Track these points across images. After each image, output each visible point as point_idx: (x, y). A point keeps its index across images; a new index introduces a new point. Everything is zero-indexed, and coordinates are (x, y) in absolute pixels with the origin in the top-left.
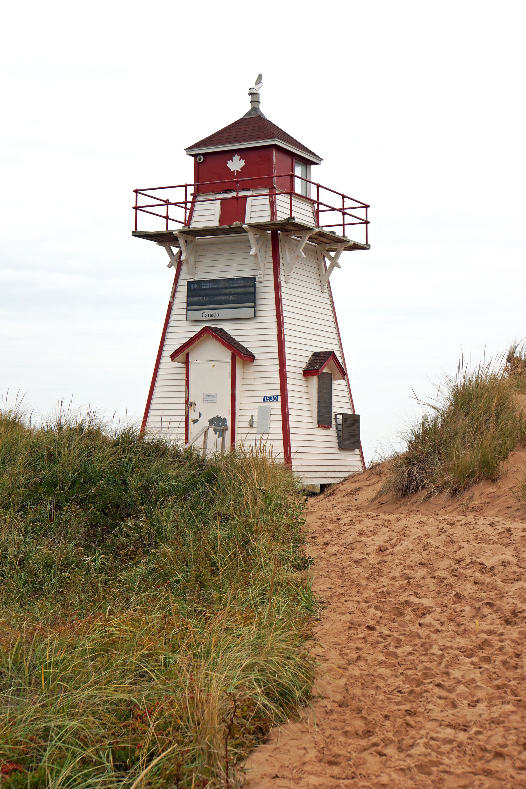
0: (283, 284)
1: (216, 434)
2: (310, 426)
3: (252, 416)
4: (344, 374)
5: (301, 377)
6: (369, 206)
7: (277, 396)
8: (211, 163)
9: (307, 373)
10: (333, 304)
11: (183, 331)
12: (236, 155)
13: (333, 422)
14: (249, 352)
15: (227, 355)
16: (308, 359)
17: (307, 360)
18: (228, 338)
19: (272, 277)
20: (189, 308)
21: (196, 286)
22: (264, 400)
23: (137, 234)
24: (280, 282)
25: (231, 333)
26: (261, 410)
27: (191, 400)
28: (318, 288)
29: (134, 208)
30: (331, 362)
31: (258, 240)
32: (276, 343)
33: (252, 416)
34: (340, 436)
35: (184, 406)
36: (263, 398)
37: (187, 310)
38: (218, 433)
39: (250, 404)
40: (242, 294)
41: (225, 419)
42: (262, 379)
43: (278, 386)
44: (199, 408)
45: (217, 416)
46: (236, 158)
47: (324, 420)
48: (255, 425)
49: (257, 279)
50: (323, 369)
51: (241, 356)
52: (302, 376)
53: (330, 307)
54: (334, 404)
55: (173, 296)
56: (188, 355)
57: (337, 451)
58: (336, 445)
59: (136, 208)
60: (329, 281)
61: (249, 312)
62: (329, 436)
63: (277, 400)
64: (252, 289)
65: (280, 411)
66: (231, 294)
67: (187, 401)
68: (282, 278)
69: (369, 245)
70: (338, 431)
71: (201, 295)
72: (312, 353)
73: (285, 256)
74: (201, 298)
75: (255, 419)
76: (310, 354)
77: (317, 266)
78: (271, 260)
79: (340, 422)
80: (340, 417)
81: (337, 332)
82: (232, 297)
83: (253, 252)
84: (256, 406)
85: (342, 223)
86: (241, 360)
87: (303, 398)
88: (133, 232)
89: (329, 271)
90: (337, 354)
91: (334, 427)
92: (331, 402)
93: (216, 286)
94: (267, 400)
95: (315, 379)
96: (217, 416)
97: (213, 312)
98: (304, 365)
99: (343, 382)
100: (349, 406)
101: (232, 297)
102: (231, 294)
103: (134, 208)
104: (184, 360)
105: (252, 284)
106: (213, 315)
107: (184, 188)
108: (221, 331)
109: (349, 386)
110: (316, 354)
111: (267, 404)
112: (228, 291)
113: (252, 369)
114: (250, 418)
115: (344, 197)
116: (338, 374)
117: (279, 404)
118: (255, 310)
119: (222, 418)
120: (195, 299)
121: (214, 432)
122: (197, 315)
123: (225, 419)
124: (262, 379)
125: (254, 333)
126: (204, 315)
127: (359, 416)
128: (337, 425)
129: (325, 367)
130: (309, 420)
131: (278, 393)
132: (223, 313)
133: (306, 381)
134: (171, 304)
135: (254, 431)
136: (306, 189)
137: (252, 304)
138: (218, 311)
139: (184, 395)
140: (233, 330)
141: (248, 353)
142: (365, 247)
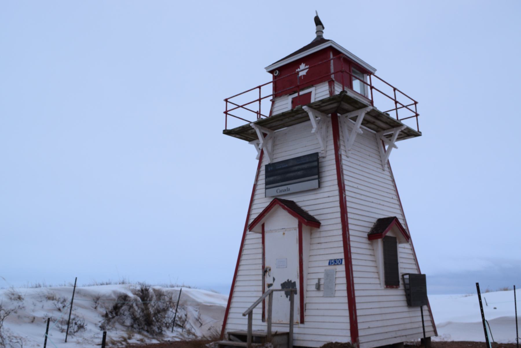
0: (343, 157)
1: (287, 297)
2: (379, 287)
3: (319, 280)
4: (407, 237)
5: (366, 241)
7: (342, 259)
8: (284, 77)
10: (393, 181)
11: (262, 203)
12: (302, 64)
13: (401, 282)
15: (293, 222)
16: (373, 224)
17: (372, 225)
19: (333, 152)
20: (268, 186)
21: (272, 168)
22: (329, 264)
23: (227, 132)
24: (341, 155)
25: (300, 204)
26: (328, 274)
27: (267, 265)
28: (380, 166)
30: (396, 228)
31: (318, 123)
32: (339, 209)
33: (319, 279)
34: (408, 290)
35: (261, 272)
36: (328, 262)
37: (266, 189)
38: (289, 296)
39: (318, 267)
40: (309, 168)
41: (295, 283)
42: (328, 244)
43: (342, 250)
44: (274, 272)
45: (288, 280)
46: (303, 66)
47: (391, 279)
48: (322, 288)
49: (320, 155)
50: (387, 232)
51: (308, 222)
52: (367, 240)
53: (398, 207)
54: (400, 265)
55: (257, 180)
56: (263, 226)
57: (406, 309)
58: (405, 303)
59: (226, 113)
60: (388, 161)
61: (315, 183)
62: (397, 295)
63: (341, 263)
64: (315, 164)
65: (344, 274)
66: (298, 170)
67: (263, 267)
68: (342, 152)
69: (421, 133)
70: (406, 290)
71: (276, 174)
73: (344, 132)
74: (275, 177)
75: (322, 282)
76: (375, 221)
78: (331, 137)
79: (407, 281)
80: (407, 277)
82: (299, 173)
83: (313, 131)
84: (322, 270)
85: (395, 108)
87: (368, 262)
88: (224, 131)
89: (387, 152)
90: (399, 217)
91: (401, 286)
93: (287, 165)
94: (332, 263)
95: (379, 244)
96: (288, 280)
98: (369, 230)
99: (407, 246)
100: (415, 267)
101: (299, 173)
102: (298, 170)
104: (261, 231)
105: (315, 159)
106: (285, 190)
107: (258, 89)
108: (292, 203)
109: (413, 249)
110: (380, 221)
111: (332, 267)
112: (296, 168)
113: (317, 235)
114: (316, 281)
115: (395, 89)
116: (401, 236)
117: (342, 268)
118: (319, 181)
119: (293, 282)
120: (271, 179)
121: (285, 296)
122: (274, 192)
123: (295, 283)
124: (328, 244)
125: (320, 202)
126: (278, 191)
127: (424, 276)
128: (405, 284)
129: (389, 233)
130: (377, 281)
131: (342, 256)
132: (294, 188)
133: (371, 244)
134: (255, 186)
135: (321, 294)
136: (364, 89)
137: (317, 176)
138: (289, 186)
139: (261, 261)
140: (305, 202)
142: (417, 134)
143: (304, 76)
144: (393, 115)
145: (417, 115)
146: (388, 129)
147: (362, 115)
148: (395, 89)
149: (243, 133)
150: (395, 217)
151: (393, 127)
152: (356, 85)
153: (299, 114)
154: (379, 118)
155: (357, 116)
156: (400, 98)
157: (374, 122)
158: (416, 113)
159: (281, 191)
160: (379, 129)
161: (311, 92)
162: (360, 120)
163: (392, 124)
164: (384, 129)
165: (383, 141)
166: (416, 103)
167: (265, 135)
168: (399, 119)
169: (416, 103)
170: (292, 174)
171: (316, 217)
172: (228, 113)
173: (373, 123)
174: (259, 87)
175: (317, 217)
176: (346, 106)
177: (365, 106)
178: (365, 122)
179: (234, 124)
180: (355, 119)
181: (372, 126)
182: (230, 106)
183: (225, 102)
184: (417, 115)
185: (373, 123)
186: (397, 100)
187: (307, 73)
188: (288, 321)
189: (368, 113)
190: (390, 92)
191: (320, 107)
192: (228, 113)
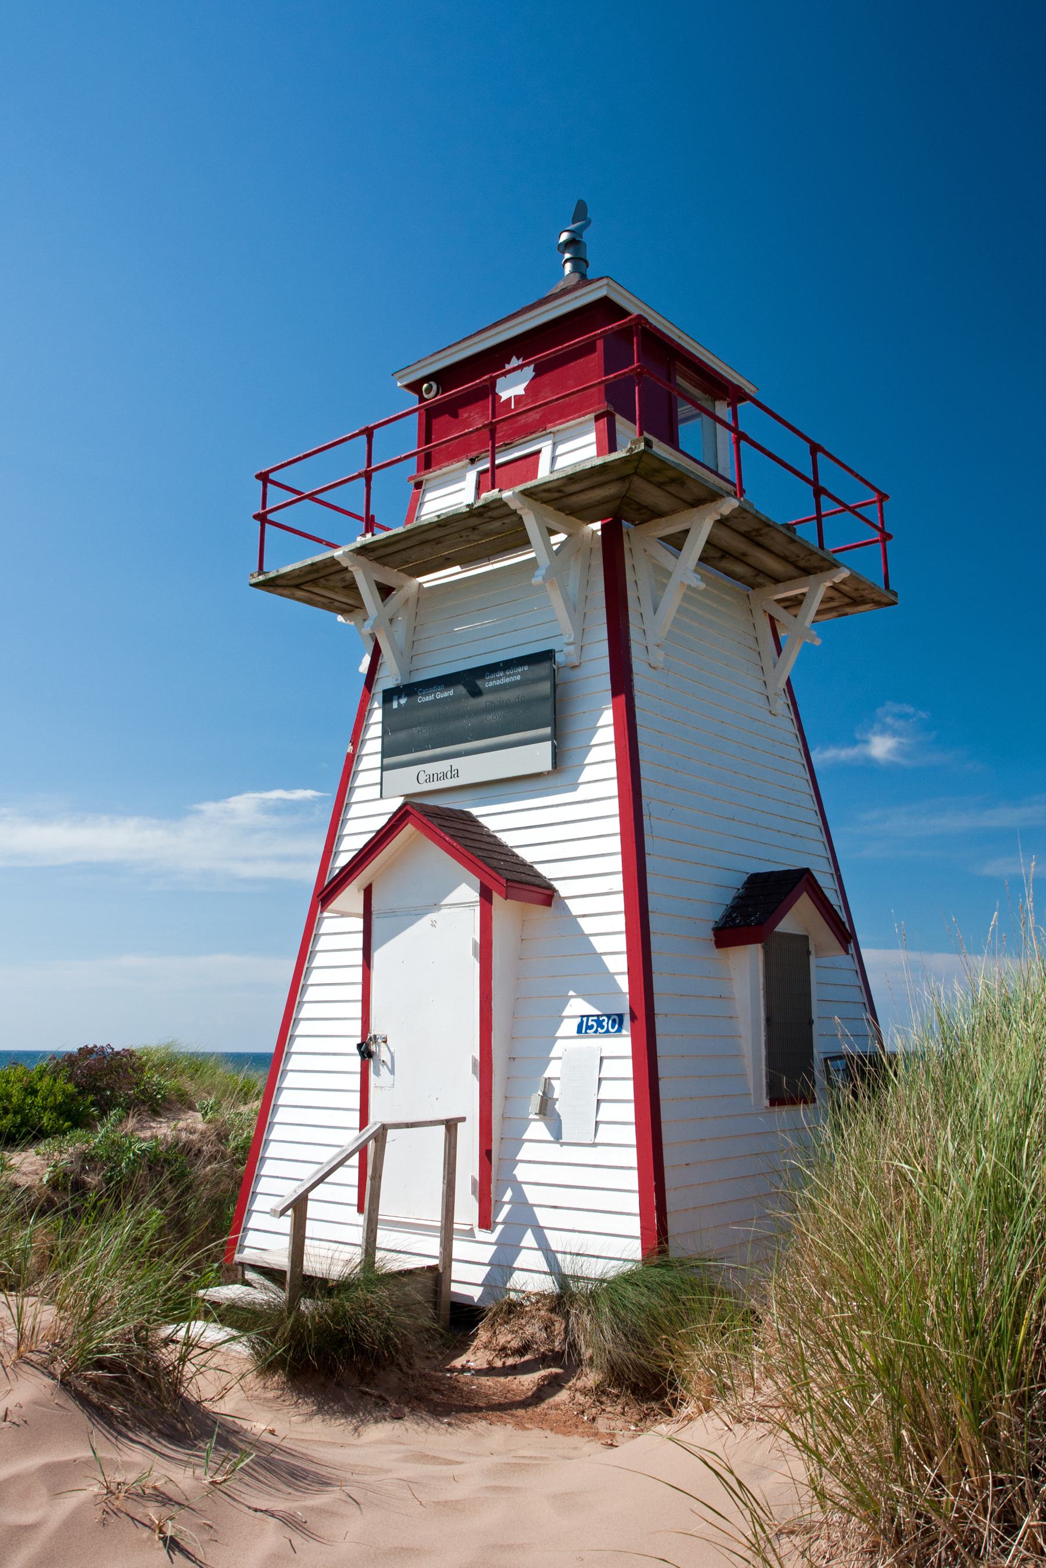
6: (886, 497)
9: (729, 932)
14: (538, 876)
16: (724, 907)
18: (497, 849)
20: (388, 761)
22: (579, 1031)
23: (270, 585)
27: (375, 1030)
29: (256, 517)
30: (804, 904)
37: (384, 768)
59: (262, 518)
61: (538, 756)
72: (745, 878)
74: (415, 730)
77: (754, 645)
81: (820, 823)
82: (491, 718)
86: (500, 894)
92: (811, 1022)
97: (443, 766)
103: (256, 517)
106: (445, 776)
115: (815, 449)
118: (554, 748)
120: (402, 735)
122: (410, 780)
126: (422, 778)
137: (548, 730)
138: (456, 762)
141: (537, 881)
143: (518, 398)
144: (807, 533)
145: (886, 537)
146: (790, 579)
147: (702, 527)
148: (815, 449)
149: (321, 585)
150: (807, 871)
151: (807, 572)
152: (692, 431)
153: (494, 519)
154: (760, 539)
155: (687, 531)
156: (830, 476)
157: (744, 554)
158: (881, 530)
159: (430, 779)
160: (760, 580)
161: (539, 452)
162: (695, 546)
163: (802, 563)
164: (777, 580)
165: (772, 619)
166: (883, 497)
167: (385, 591)
168: (829, 547)
169: (883, 497)
170: (468, 723)
171: (543, 870)
172: (270, 517)
173: (740, 558)
174: (369, 432)
175: (546, 871)
176: (651, 495)
177: (714, 496)
178: (714, 555)
179: (290, 558)
180: (676, 542)
181: (739, 569)
182: (276, 496)
183: (260, 483)
184: (886, 537)
185: (740, 558)
186: (822, 483)
187: (525, 390)
188: (435, 1216)
189: (722, 522)
190: (800, 456)
191: (564, 497)
192: (270, 517)
